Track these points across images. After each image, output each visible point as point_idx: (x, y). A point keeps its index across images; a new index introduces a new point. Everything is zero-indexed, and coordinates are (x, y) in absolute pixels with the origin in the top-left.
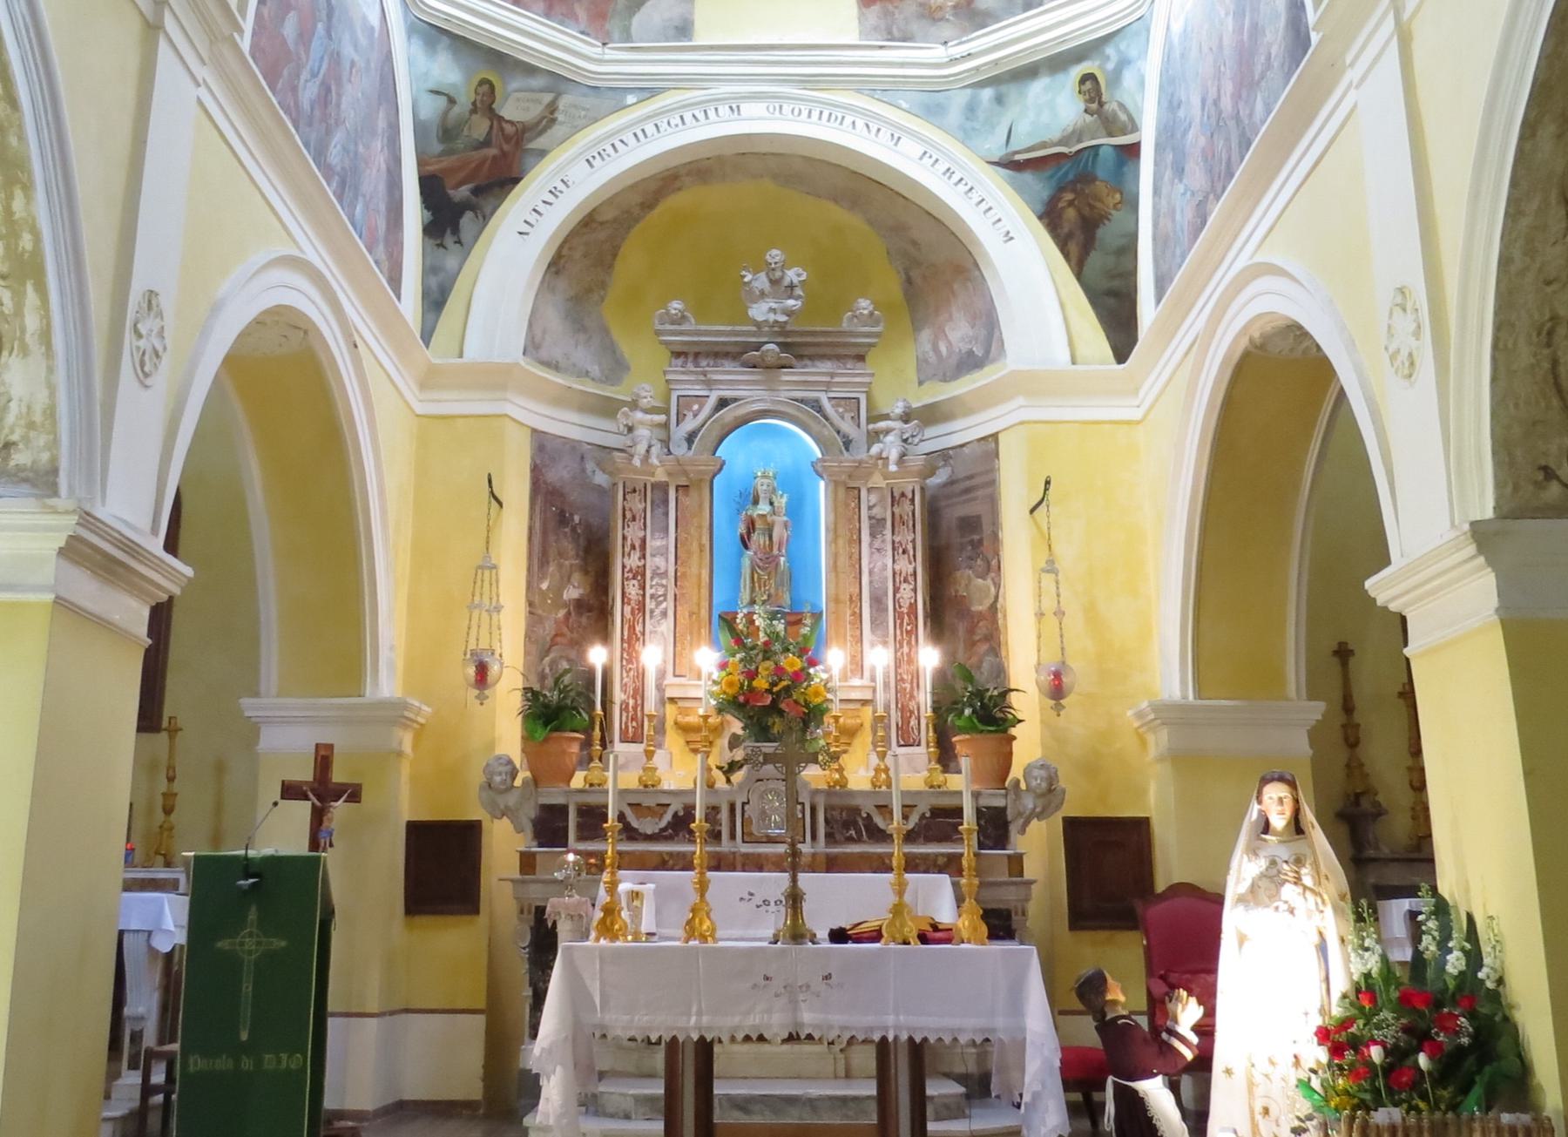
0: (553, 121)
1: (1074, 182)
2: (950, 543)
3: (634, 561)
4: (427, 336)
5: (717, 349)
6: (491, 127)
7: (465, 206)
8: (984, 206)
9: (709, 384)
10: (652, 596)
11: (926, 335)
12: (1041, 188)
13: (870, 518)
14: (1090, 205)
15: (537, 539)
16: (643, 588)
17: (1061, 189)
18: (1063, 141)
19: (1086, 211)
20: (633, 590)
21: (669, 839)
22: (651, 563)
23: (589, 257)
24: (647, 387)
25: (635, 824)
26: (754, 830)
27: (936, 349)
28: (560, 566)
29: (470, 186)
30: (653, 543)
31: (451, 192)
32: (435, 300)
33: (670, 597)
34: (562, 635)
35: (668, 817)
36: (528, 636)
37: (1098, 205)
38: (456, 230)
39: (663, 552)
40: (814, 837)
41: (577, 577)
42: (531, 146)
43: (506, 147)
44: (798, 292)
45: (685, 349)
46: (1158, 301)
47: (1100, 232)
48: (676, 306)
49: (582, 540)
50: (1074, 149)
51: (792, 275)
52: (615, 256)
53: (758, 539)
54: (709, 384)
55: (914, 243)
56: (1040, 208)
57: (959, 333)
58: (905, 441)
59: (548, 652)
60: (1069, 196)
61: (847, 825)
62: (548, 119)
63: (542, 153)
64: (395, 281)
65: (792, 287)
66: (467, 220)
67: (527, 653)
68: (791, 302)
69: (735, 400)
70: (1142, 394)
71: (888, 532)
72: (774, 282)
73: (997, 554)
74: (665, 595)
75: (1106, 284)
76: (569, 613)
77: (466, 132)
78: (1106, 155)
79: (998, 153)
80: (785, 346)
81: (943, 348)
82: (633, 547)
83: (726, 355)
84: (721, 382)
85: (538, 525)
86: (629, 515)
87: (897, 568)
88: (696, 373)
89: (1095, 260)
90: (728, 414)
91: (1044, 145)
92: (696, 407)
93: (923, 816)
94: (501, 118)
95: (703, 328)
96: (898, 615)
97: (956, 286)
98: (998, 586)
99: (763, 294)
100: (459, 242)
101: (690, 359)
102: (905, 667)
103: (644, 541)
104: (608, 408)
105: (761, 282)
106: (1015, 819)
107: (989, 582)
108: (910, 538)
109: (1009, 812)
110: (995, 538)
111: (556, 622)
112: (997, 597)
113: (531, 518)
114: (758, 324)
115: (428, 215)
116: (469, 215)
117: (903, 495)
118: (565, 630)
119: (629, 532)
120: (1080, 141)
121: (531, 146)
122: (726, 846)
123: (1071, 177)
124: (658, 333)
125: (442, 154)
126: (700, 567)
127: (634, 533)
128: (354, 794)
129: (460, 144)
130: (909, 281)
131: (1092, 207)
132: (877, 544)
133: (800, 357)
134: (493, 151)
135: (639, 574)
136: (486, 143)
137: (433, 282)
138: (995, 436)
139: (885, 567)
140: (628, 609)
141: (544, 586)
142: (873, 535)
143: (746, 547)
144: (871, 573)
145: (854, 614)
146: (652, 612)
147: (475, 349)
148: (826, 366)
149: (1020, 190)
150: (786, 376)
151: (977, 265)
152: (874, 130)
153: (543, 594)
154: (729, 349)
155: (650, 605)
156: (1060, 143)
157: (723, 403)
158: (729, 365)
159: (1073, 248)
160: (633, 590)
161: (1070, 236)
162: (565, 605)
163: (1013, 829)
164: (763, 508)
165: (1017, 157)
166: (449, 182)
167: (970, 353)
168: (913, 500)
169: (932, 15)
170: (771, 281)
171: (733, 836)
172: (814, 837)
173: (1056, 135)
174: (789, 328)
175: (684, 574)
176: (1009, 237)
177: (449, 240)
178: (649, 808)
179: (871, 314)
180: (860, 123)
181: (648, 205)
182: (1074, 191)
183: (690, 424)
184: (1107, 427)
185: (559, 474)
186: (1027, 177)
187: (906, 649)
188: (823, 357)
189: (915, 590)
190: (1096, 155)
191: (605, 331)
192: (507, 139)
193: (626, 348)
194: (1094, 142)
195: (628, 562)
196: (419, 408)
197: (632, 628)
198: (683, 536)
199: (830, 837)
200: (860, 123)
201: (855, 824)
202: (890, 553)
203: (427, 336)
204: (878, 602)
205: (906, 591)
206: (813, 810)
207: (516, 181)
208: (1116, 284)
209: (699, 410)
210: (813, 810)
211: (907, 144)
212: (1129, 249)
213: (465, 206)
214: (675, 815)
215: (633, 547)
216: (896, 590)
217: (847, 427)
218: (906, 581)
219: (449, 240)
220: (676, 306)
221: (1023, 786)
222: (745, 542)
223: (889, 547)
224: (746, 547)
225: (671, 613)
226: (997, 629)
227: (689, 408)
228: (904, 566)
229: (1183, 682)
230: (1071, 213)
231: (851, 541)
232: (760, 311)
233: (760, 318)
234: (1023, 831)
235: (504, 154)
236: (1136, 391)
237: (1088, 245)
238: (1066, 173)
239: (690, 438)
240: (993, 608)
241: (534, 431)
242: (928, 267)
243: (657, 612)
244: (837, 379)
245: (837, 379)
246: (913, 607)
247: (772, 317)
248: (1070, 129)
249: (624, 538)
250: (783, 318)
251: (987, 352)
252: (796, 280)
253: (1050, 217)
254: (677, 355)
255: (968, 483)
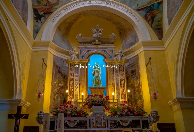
0: (59, 3)
1: (150, 11)
2: (131, 74)
3: (72, 78)
4: (34, 37)
5: (87, 42)
6: (47, 3)
7: (42, 16)
8: (134, 16)
9: (86, 48)
10: (75, 84)
11: (123, 42)
12: (143, 13)
13: (116, 70)
14: (153, 14)
15: (54, 74)
16: (74, 82)
17: (147, 13)
18: (147, 4)
19: (152, 15)
20: (72, 83)
21: (76, 128)
22: (75, 78)
23: (66, 28)
24: (75, 47)
25: (69, 125)
26: (94, 125)
27: (126, 44)
28: (59, 80)
29: (43, 12)
30: (76, 75)
31: (39, 13)
32: (36, 31)
33: (79, 84)
34: (59, 92)
35: (76, 123)
36: (51, 91)
37: (155, 14)
38: (40, 20)
39: (77, 76)
40: (107, 127)
41: (62, 82)
42: (54, 7)
43: (50, 7)
44: (101, 32)
45: (82, 42)
46: (169, 24)
47: (155, 19)
48: (80, 34)
49: (62, 75)
50: (149, 5)
51: (100, 29)
52: (70, 29)
53: (96, 75)
54: (86, 48)
55: (121, 26)
56: (144, 16)
57: (129, 40)
58: (121, 56)
59: (56, 95)
60: (149, 14)
61: (114, 124)
62: (58, 3)
63: (57, 9)
64: (26, 23)
65: (100, 31)
66: (42, 18)
67: (51, 94)
68: (100, 33)
69: (91, 50)
70: (165, 46)
71: (119, 72)
72: (97, 30)
73: (139, 75)
74: (78, 84)
75: (156, 27)
76: (60, 88)
77: (42, 3)
78: (156, 5)
79: (136, 8)
80: (99, 41)
81: (127, 43)
82: (72, 75)
83: (89, 43)
84: (88, 47)
85: (54, 72)
86: (71, 69)
87: (121, 78)
88: (84, 46)
89: (154, 24)
90: (90, 53)
91: (144, 6)
92: (84, 51)
93: (130, 122)
94: (49, 2)
95: (85, 38)
96: (122, 87)
97: (129, 32)
98: (140, 81)
99: (95, 33)
100: (41, 22)
101: (83, 44)
102: (123, 96)
103: (74, 74)
104: (67, 53)
105: (95, 31)
106: (150, 123)
107: (138, 81)
108: (123, 73)
109: (149, 121)
110: (139, 73)
111: (58, 89)
112: (140, 83)
113: (53, 70)
114: (95, 37)
115: (35, 16)
116: (43, 17)
117: (121, 65)
118: (59, 91)
119: (71, 72)
120: (150, 3)
121: (54, 7)
122: (88, 129)
123: (149, 10)
124: (77, 39)
125: (37, 5)
126: (84, 79)
127: (72, 73)
128: (10, 116)
129: (41, 5)
130: (120, 33)
131: (153, 15)
132: (117, 74)
133: (102, 43)
134: (47, 7)
135: (73, 80)
136: (46, 5)
137: (36, 28)
138: (138, 55)
139: (118, 78)
140: (71, 86)
141: (55, 83)
142: (116, 73)
143: (94, 76)
144: (116, 79)
145: (113, 87)
146: (75, 87)
147: (43, 39)
148: (107, 45)
149: (140, 14)
150: (100, 46)
151: (133, 27)
152: (114, 5)
153: (55, 84)
154: (90, 42)
155: (75, 85)
156: (147, 5)
157: (88, 51)
158: (89, 44)
159: (150, 22)
160: (72, 83)
161: (149, 20)
162: (59, 87)
163: (150, 125)
164: (96, 69)
165: (139, 9)
166: (39, 11)
167: (132, 43)
168: (123, 66)
169: (123, 2)
170: (97, 30)
171: (90, 127)
172: (107, 127)
173: (146, 4)
174: (100, 38)
175: (81, 80)
176: (138, 21)
177: (39, 21)
178: (72, 121)
179: (114, 35)
180: (112, 4)
181: (75, 20)
182: (150, 12)
183: (82, 54)
184: (159, 51)
185: (58, 64)
186: (141, 11)
187: (123, 93)
188: (106, 43)
189: (124, 82)
190: (154, 5)
191: (68, 42)
192: (50, 6)
193: (72, 45)
194: (153, 3)
195: (71, 78)
196: (32, 50)
197: (71, 90)
198: (81, 73)
199: (111, 127)
200: (112, 4)
201: (116, 124)
202: (119, 76)
203: (34, 37)
204: (117, 85)
205: (123, 83)
206: (107, 121)
207: (52, 13)
208: (159, 27)
209: (84, 52)
210: (107, 121)
211: (120, 7)
212: (161, 20)
213: (42, 16)
214: (78, 123)
215: (72, 75)
216: (121, 82)
217: (111, 54)
218: (123, 80)
219: (39, 21)
220: (80, 34)
221: (151, 116)
222: (94, 75)
223: (119, 75)
224: (94, 76)
225: (79, 87)
226: (140, 89)
227: (82, 51)
228: (122, 78)
229: (182, 94)
230: (149, 16)
231: (112, 74)
232: (94, 35)
233: (95, 36)
234: (151, 125)
235: (50, 8)
236: (163, 45)
237: (153, 21)
238: (148, 10)
239: (83, 57)
240: (139, 85)
241: (54, 55)
242: (124, 29)
243: (76, 87)
244: (109, 47)
245: (109, 47)
246: (124, 85)
247: (97, 36)
248: (149, 2)
249: (70, 73)
250: (99, 36)
251: (135, 41)
252: (101, 30)
253: (145, 17)
254: (80, 43)
255: (133, 64)
